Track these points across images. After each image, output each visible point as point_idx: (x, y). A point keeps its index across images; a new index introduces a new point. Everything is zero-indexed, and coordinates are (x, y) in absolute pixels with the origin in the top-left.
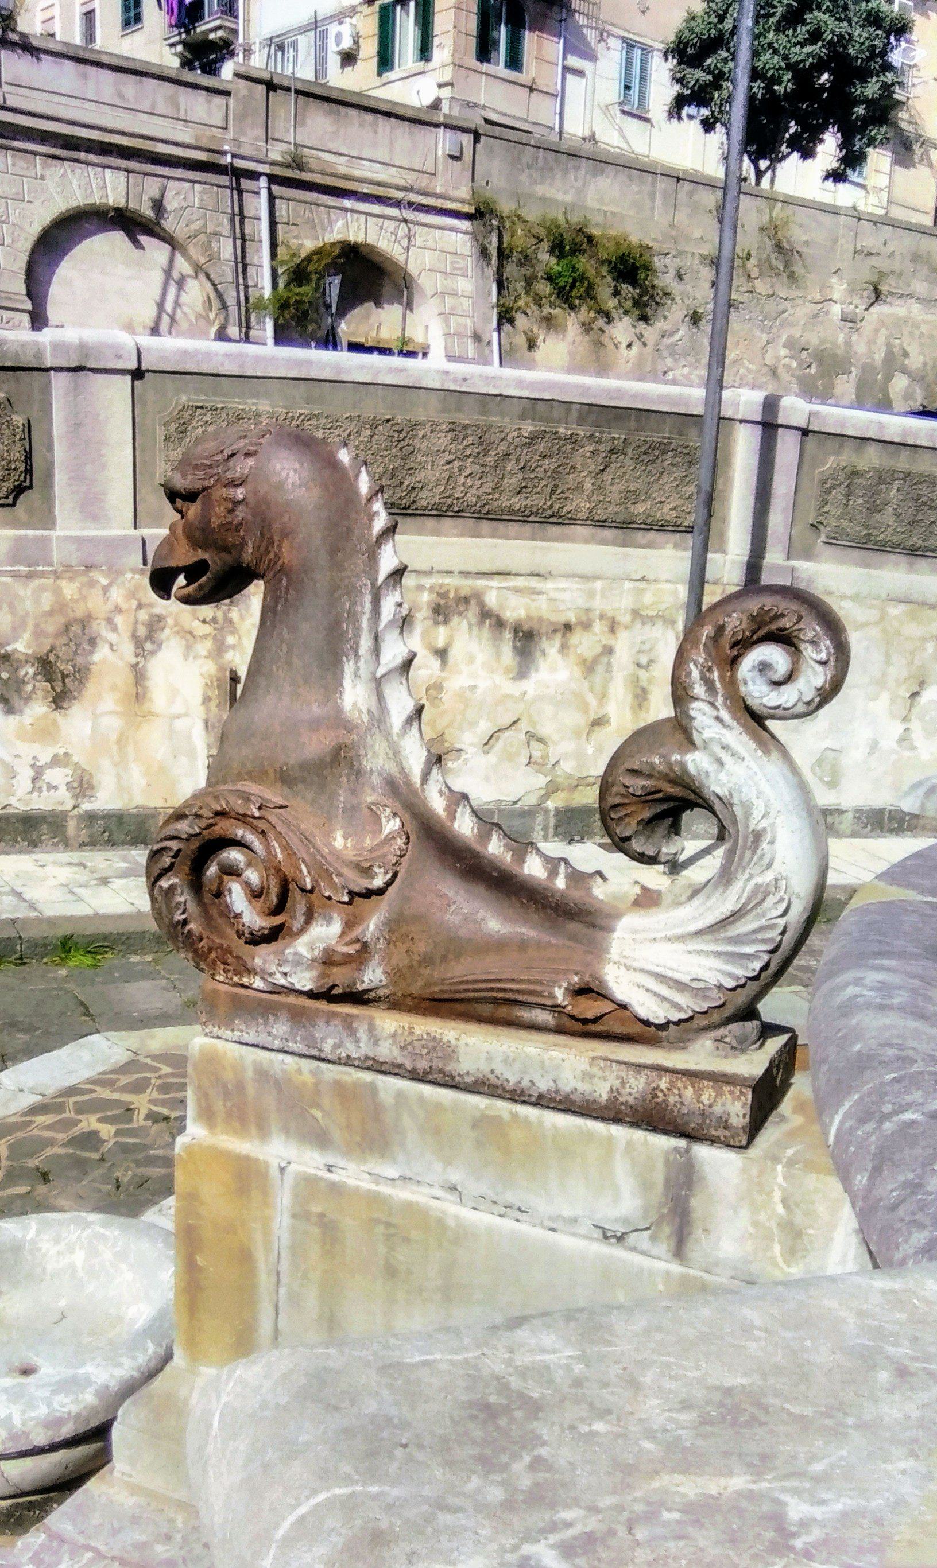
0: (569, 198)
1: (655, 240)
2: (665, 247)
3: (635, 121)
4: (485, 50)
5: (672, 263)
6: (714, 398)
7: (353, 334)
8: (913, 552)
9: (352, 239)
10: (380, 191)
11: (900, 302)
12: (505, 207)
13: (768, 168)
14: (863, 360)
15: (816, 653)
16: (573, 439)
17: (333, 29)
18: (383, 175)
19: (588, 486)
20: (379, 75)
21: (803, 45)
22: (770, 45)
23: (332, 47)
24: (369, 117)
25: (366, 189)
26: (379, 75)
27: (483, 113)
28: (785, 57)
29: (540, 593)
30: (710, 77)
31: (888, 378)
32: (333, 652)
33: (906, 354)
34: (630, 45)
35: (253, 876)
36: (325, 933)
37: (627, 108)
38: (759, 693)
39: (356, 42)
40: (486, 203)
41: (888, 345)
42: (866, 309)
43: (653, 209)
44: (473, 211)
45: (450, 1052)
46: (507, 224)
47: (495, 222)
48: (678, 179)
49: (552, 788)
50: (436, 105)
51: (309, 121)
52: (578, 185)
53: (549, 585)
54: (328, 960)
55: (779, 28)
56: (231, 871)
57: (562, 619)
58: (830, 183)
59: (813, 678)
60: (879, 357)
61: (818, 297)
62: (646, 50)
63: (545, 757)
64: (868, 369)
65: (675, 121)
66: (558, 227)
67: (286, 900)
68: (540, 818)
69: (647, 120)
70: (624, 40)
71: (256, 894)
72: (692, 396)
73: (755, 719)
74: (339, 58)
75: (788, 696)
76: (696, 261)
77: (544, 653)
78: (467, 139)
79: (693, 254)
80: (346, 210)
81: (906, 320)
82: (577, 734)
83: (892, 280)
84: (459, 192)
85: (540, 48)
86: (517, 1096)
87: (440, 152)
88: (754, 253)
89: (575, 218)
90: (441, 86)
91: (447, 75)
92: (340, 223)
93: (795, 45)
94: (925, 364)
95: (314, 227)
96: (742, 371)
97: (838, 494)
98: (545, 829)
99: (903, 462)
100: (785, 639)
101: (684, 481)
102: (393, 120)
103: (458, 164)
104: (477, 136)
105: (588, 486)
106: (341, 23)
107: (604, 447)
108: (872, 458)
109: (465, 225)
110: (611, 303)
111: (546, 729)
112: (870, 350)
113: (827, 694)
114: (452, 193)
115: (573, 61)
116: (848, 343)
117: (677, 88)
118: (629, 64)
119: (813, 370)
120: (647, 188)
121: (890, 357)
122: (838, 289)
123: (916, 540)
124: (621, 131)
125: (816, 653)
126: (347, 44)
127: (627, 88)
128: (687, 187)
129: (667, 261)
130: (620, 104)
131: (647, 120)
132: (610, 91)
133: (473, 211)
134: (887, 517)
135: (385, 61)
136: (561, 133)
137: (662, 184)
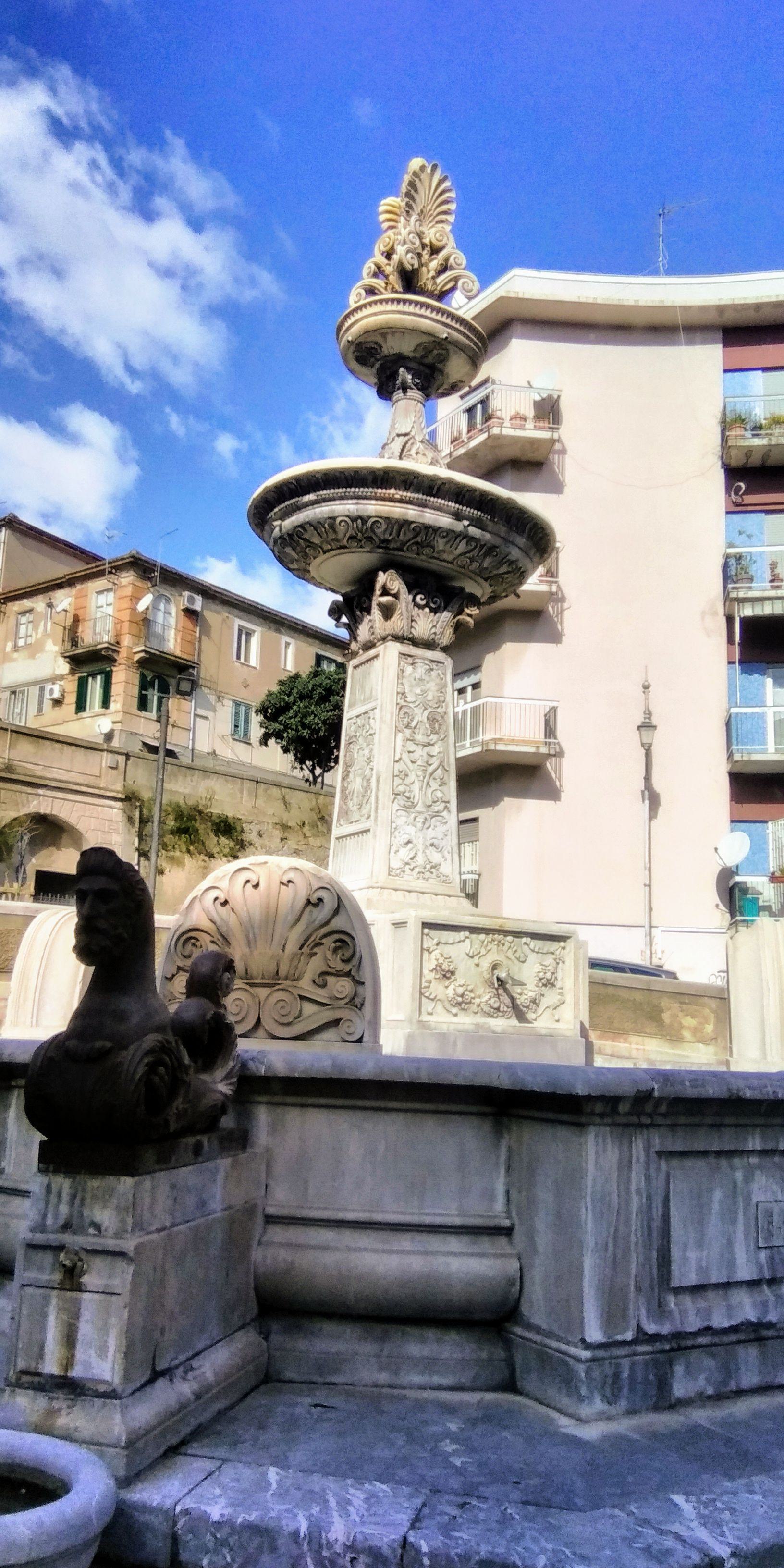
0: (187, 791)
1: (243, 815)
2: (250, 819)
3: (242, 744)
4: (143, 704)
5: (255, 828)
7: (40, 865)
9: (42, 811)
10: (63, 785)
12: (146, 795)
17: (48, 687)
18: (65, 776)
20: (76, 713)
22: (313, 712)
23: (47, 696)
24: (58, 745)
25: (54, 784)
26: (76, 713)
27: (141, 738)
30: (282, 727)
34: (237, 704)
37: (236, 737)
39: (63, 695)
40: (133, 793)
43: (242, 798)
44: (124, 797)
46: (146, 804)
47: (138, 804)
48: (257, 782)
50: (109, 737)
51: (19, 747)
52: (194, 784)
55: (317, 704)
62: (248, 707)
65: (264, 747)
66: (179, 806)
69: (250, 744)
70: (234, 701)
74: (51, 702)
76: (271, 826)
78: (122, 759)
79: (268, 823)
80: (40, 795)
84: (117, 787)
85: (179, 705)
87: (104, 765)
89: (191, 802)
90: (114, 723)
91: (119, 717)
92: (35, 802)
95: (17, 804)
102: (74, 747)
103: (114, 771)
104: (128, 756)
106: (54, 684)
109: (119, 804)
110: (215, 850)
114: (110, 787)
115: (200, 712)
117: (263, 730)
118: (237, 714)
120: (239, 786)
124: (233, 750)
126: (56, 695)
127: (236, 726)
129: (251, 826)
130: (232, 735)
131: (250, 744)
132: (227, 727)
133: (124, 797)
135: (81, 706)
136: (193, 750)
137: (247, 784)
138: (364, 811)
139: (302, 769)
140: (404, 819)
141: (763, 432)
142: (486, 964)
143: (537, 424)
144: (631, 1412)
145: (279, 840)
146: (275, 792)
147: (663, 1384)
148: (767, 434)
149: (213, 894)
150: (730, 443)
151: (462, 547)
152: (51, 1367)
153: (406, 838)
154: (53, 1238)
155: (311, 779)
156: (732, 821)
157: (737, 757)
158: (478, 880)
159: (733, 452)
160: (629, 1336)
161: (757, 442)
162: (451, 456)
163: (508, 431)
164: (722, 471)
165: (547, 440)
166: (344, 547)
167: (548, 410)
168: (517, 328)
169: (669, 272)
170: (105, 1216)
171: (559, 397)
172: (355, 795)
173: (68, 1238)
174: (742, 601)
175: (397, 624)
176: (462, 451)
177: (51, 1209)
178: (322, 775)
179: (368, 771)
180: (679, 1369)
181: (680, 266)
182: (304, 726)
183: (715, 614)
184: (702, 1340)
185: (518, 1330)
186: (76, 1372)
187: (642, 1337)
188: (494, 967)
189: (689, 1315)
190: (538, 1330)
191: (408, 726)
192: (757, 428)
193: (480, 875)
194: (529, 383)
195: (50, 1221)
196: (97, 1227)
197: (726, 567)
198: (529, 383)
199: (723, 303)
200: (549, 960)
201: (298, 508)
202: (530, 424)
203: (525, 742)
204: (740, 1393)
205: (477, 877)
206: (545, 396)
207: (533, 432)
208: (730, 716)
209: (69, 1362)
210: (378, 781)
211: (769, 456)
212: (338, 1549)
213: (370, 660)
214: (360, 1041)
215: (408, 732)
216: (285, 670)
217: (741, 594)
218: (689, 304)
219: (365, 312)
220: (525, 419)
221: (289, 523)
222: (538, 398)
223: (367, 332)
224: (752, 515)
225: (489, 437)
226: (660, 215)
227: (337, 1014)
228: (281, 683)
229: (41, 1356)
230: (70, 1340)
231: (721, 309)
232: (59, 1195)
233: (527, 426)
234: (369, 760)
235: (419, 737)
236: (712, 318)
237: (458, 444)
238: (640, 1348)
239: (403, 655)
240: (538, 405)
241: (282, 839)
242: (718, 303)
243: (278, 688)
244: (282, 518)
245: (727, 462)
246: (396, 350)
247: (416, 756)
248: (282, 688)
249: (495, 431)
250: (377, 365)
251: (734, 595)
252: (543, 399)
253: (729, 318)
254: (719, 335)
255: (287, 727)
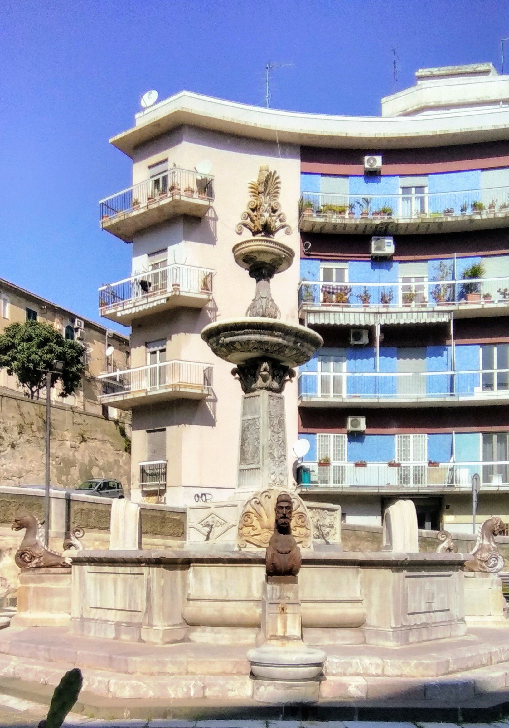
6: (48, 492)
8: (99, 528)
11: (92, 441)
13: (36, 391)
14: (81, 461)
15: (82, 532)
16: (9, 502)
19: (14, 514)
21: (47, 354)
28: (41, 357)
29: (3, 540)
31: (91, 468)
32: (35, 534)
33: (97, 460)
35: (28, 556)
36: (36, 561)
38: (77, 536)
41: (90, 457)
42: (80, 443)
45: (50, 571)
49: (8, 593)
53: (5, 538)
54: (37, 563)
56: (26, 556)
57: (9, 547)
58: (61, 397)
59: (81, 534)
60: (86, 460)
61: (61, 439)
63: (6, 584)
64: (82, 464)
67: (33, 557)
68: (5, 601)
71: (28, 558)
72: (42, 492)
73: (77, 538)
75: (80, 536)
77: (4, 556)
81: (96, 447)
82: (14, 577)
83: (88, 433)
86: (58, 574)
88: (35, 423)
93: (44, 354)
94: (104, 463)
96: (33, 465)
97: (79, 514)
98: (7, 604)
99: (94, 507)
100: (79, 531)
101: (39, 512)
105: (14, 514)
107: (18, 504)
108: (86, 506)
111: (6, 576)
112: (82, 458)
113: (83, 536)
116: (74, 456)
119: (62, 465)
121: (90, 461)
122: (68, 435)
123: (100, 526)
125: (82, 532)
128: (5, 399)
134: (92, 520)
138: (256, 460)
139: (24, 386)
140: (272, 464)
141: (322, 214)
142: (315, 520)
143: (200, 196)
144: (401, 645)
145: (17, 434)
146: (13, 402)
147: (407, 638)
148: (323, 216)
149: (255, 500)
150: (305, 219)
151: (294, 352)
152: (280, 633)
153: (272, 471)
154: (277, 601)
155: (30, 392)
156: (299, 433)
157: (304, 399)
158: (166, 464)
159: (306, 224)
160: (400, 626)
161: (319, 220)
162: (148, 208)
163: (184, 199)
164: (299, 233)
165: (206, 206)
166: (250, 351)
167: (206, 187)
168: (186, 132)
169: (272, 106)
170: (290, 594)
171: (212, 180)
172: (249, 453)
173: (280, 601)
174: (309, 312)
175: (268, 383)
176: (154, 206)
177: (274, 594)
178: (37, 391)
179: (256, 444)
180: (410, 634)
181: (279, 103)
182: (29, 361)
183: (293, 317)
184: (415, 627)
185: (192, 693)
186: (287, 634)
187: (404, 626)
188: (318, 521)
189: (412, 620)
190: (374, 627)
191: (272, 426)
192: (319, 211)
193: (167, 461)
194: (195, 168)
195: (274, 597)
196: (289, 598)
197: (300, 292)
198: (195, 168)
199: (302, 132)
200: (332, 518)
201: (235, 335)
202: (196, 195)
203: (192, 387)
204: (423, 641)
205: (165, 462)
206: (203, 178)
207: (198, 200)
208: (301, 376)
209: (285, 632)
210: (263, 448)
211: (324, 228)
212: (368, 664)
213: (254, 396)
214: (309, 548)
215: (272, 428)
216: (4, 318)
217: (309, 308)
218: (284, 130)
219: (252, 244)
220: (193, 192)
221: (228, 340)
222: (200, 178)
223: (252, 252)
224: (314, 261)
225: (173, 200)
226: (267, 68)
227: (302, 539)
228: (8, 329)
229: (277, 631)
230: (285, 626)
231: (301, 135)
232: (276, 590)
233: (194, 196)
234: (257, 439)
235: (276, 430)
236: (296, 140)
237: (152, 201)
238: (403, 629)
239: (269, 395)
240: (199, 182)
241: (19, 433)
242: (300, 132)
243: (5, 332)
244: (225, 337)
245: (302, 228)
246: (263, 260)
247: (275, 437)
248: (8, 332)
249: (177, 197)
250: (252, 264)
251: (305, 308)
252: (202, 179)
253: (306, 142)
254: (299, 151)
255: (14, 359)
